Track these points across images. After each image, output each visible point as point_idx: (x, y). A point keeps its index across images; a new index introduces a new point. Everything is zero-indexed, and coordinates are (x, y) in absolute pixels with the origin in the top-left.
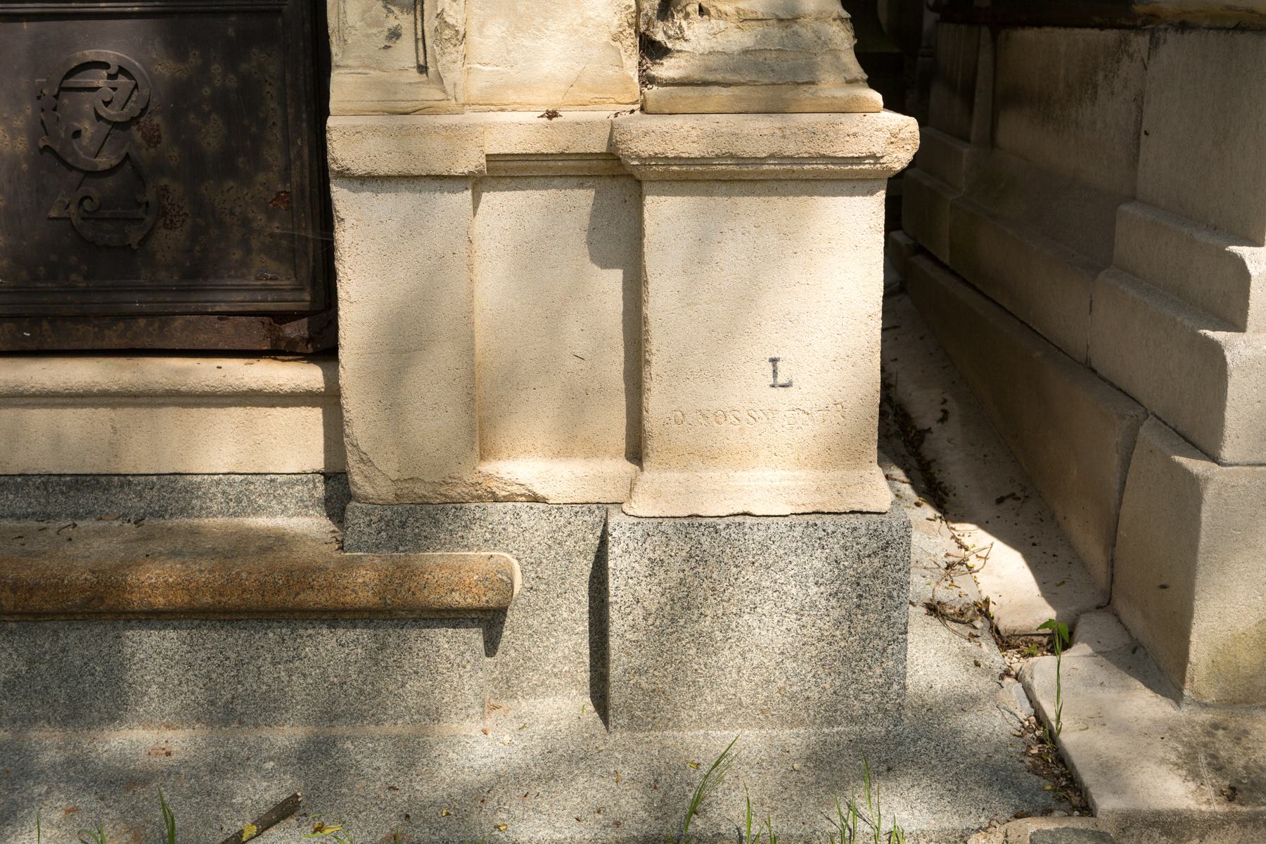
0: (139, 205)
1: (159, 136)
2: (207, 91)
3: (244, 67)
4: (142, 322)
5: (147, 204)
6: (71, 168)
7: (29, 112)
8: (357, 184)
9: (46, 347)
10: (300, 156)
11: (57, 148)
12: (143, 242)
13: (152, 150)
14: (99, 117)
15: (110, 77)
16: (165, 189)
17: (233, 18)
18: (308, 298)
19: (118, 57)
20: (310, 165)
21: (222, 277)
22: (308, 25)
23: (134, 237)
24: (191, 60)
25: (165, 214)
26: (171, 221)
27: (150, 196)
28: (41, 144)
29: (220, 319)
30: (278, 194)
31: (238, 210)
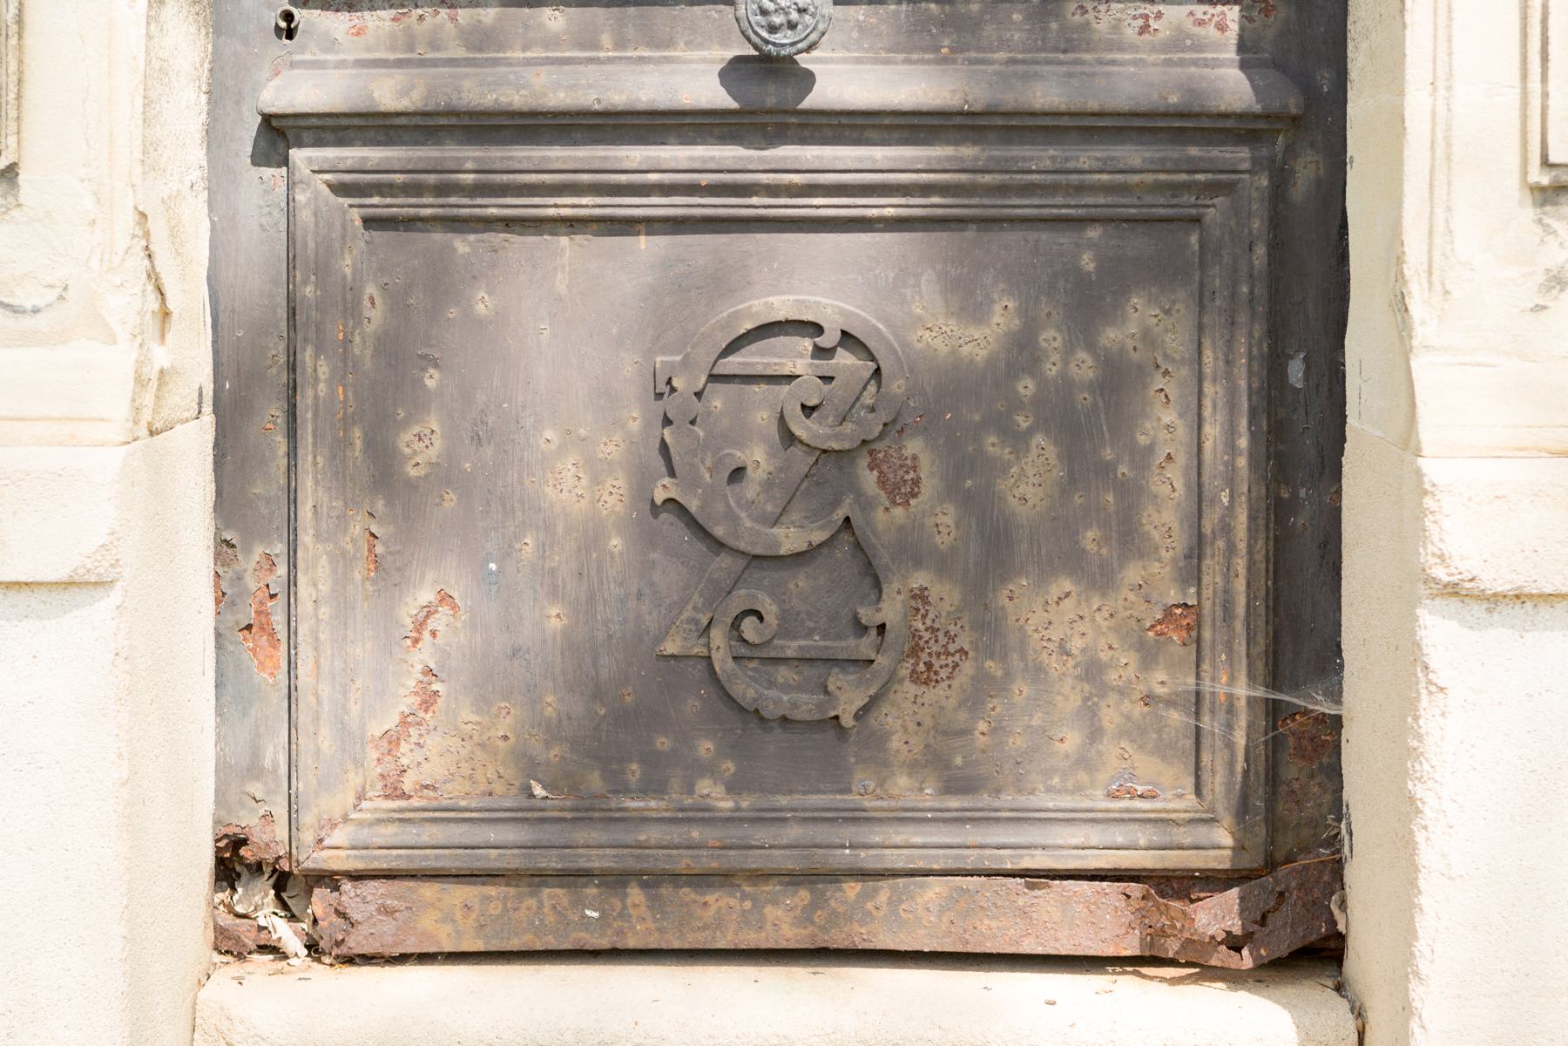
0: (862, 629)
1: (916, 482)
2: (1026, 387)
3: (1111, 336)
4: (852, 889)
5: (882, 628)
6: (718, 545)
7: (635, 426)
8: (1479, 609)
9: (632, 943)
10: (1226, 529)
11: (693, 506)
12: (862, 713)
13: (899, 512)
14: (789, 438)
15: (821, 352)
16: (921, 596)
17: (1094, 233)
18: (1228, 841)
19: (843, 313)
20: (1250, 552)
21: (1032, 792)
22: (1261, 250)
23: (847, 704)
24: (997, 319)
25: (915, 651)
26: (929, 665)
27: (891, 610)
28: (660, 496)
29: (1031, 887)
30: (1168, 611)
31: (1076, 644)
